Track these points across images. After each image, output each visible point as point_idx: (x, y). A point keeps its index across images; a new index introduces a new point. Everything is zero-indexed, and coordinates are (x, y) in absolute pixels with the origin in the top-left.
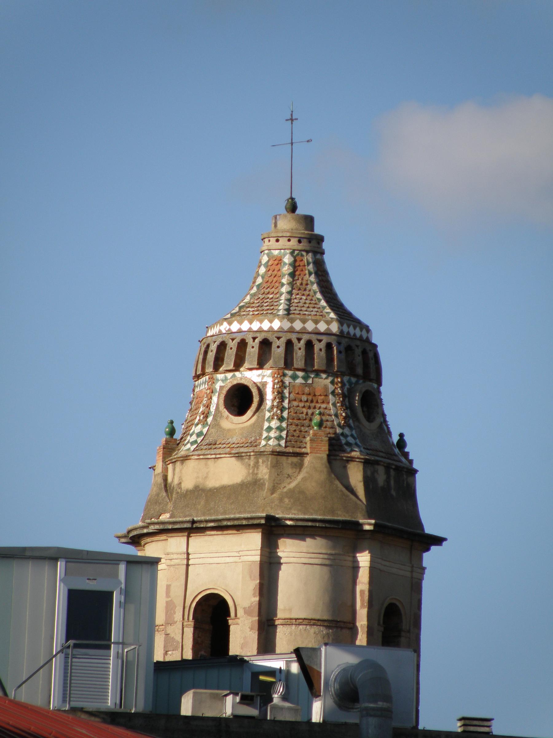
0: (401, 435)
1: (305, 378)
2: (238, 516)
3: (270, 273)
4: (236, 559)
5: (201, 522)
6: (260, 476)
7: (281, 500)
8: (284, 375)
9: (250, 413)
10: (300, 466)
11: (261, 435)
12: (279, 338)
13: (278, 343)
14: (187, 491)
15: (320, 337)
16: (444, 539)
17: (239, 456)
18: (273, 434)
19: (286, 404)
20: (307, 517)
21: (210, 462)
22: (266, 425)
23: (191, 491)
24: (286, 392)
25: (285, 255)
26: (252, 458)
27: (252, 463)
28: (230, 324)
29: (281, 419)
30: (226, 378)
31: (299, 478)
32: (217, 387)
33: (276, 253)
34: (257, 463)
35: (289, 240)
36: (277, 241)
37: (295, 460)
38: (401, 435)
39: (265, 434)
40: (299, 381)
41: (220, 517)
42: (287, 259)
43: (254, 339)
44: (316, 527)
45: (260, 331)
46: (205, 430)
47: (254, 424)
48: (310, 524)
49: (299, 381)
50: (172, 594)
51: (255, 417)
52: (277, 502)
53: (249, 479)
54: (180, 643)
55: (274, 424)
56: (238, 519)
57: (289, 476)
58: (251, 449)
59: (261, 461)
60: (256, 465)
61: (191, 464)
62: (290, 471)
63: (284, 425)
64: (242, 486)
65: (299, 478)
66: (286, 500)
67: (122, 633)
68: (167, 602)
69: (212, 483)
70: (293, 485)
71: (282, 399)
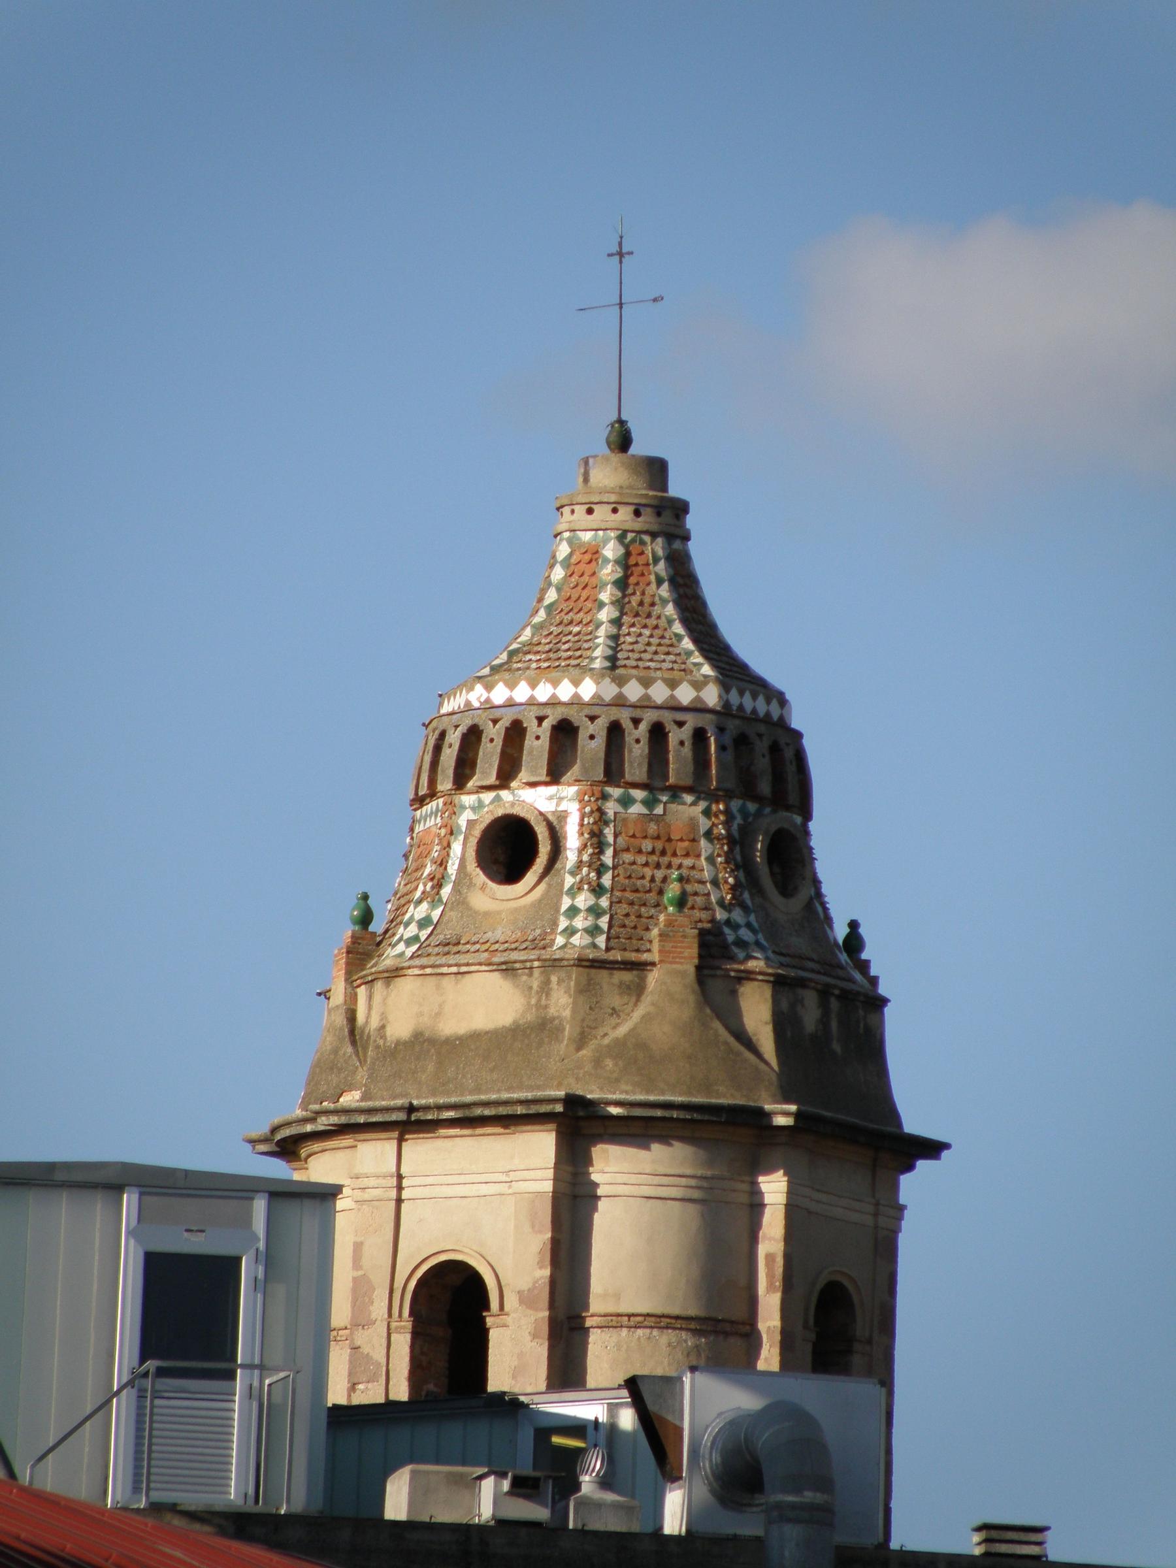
1: (649, 803)
2: (505, 1096)
4: (503, 1188)
6: (552, 1011)
7: (597, 1062)
9: (531, 877)
10: (638, 990)
11: (555, 923)
12: (592, 718)
13: (591, 728)
14: (398, 1043)
15: (680, 716)
17: (508, 969)
20: (652, 1098)
21: (446, 981)
22: (566, 903)
23: (405, 1043)
24: (609, 832)
25: (605, 541)
26: (536, 973)
27: (535, 985)
28: (489, 688)
29: (598, 890)
30: (481, 804)
31: (637, 1014)
32: (462, 821)
33: (587, 536)
34: (547, 982)
35: (615, 511)
36: (590, 511)
37: (627, 976)
39: (563, 923)
40: (637, 809)
41: (469, 1099)
42: (611, 551)
43: (541, 720)
45: (554, 703)
47: (540, 901)
49: (637, 809)
50: (365, 1262)
51: (542, 886)
52: (588, 1067)
56: (506, 1103)
57: (614, 1012)
58: (533, 955)
59: (554, 979)
60: (545, 988)
61: (406, 986)
62: (616, 1000)
63: (604, 902)
64: (516, 1032)
65: (637, 1014)
66: (609, 1063)
68: (355, 1280)
69: (451, 1027)
70: (622, 1030)
71: (600, 847)
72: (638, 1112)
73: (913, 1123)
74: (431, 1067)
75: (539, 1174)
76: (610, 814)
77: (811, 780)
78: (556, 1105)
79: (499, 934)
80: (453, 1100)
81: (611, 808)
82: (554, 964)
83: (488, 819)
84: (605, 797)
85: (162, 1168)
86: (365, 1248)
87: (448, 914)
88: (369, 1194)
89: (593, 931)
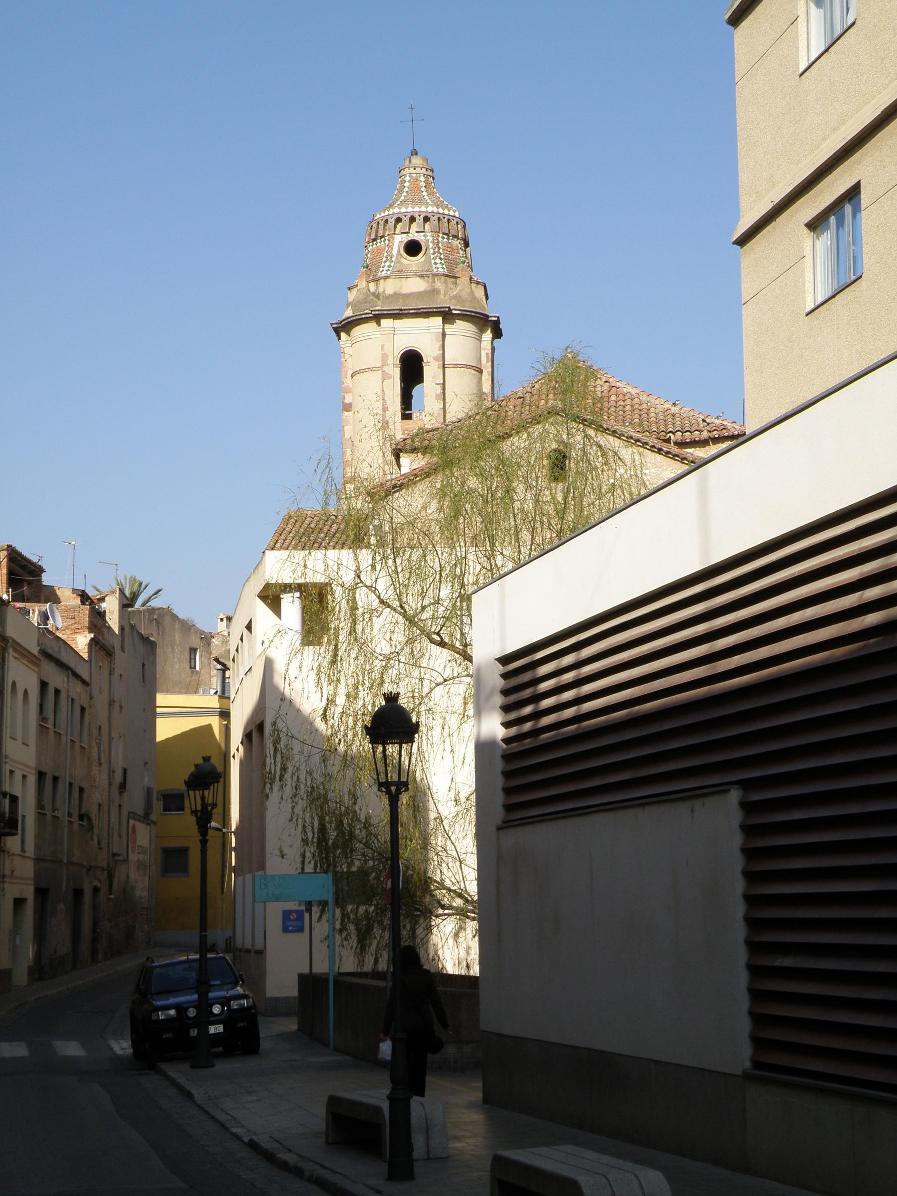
3: (412, 186)
4: (426, 331)
6: (436, 287)
9: (420, 255)
11: (432, 267)
12: (434, 216)
13: (434, 218)
14: (389, 295)
15: (444, 216)
17: (422, 276)
18: (438, 266)
20: (463, 309)
22: (433, 261)
23: (392, 295)
25: (420, 176)
26: (430, 277)
28: (400, 208)
33: (414, 175)
35: (415, 169)
36: (415, 169)
37: (453, 280)
43: (420, 216)
44: (385, 314)
45: (393, 214)
48: (469, 313)
51: (424, 258)
59: (436, 279)
60: (433, 281)
62: (452, 286)
63: (443, 262)
64: (425, 292)
66: (453, 300)
67: (763, 428)
68: (382, 354)
70: (455, 293)
75: (485, 339)
76: (440, 240)
85: (868, 536)
86: (385, 347)
87: (396, 265)
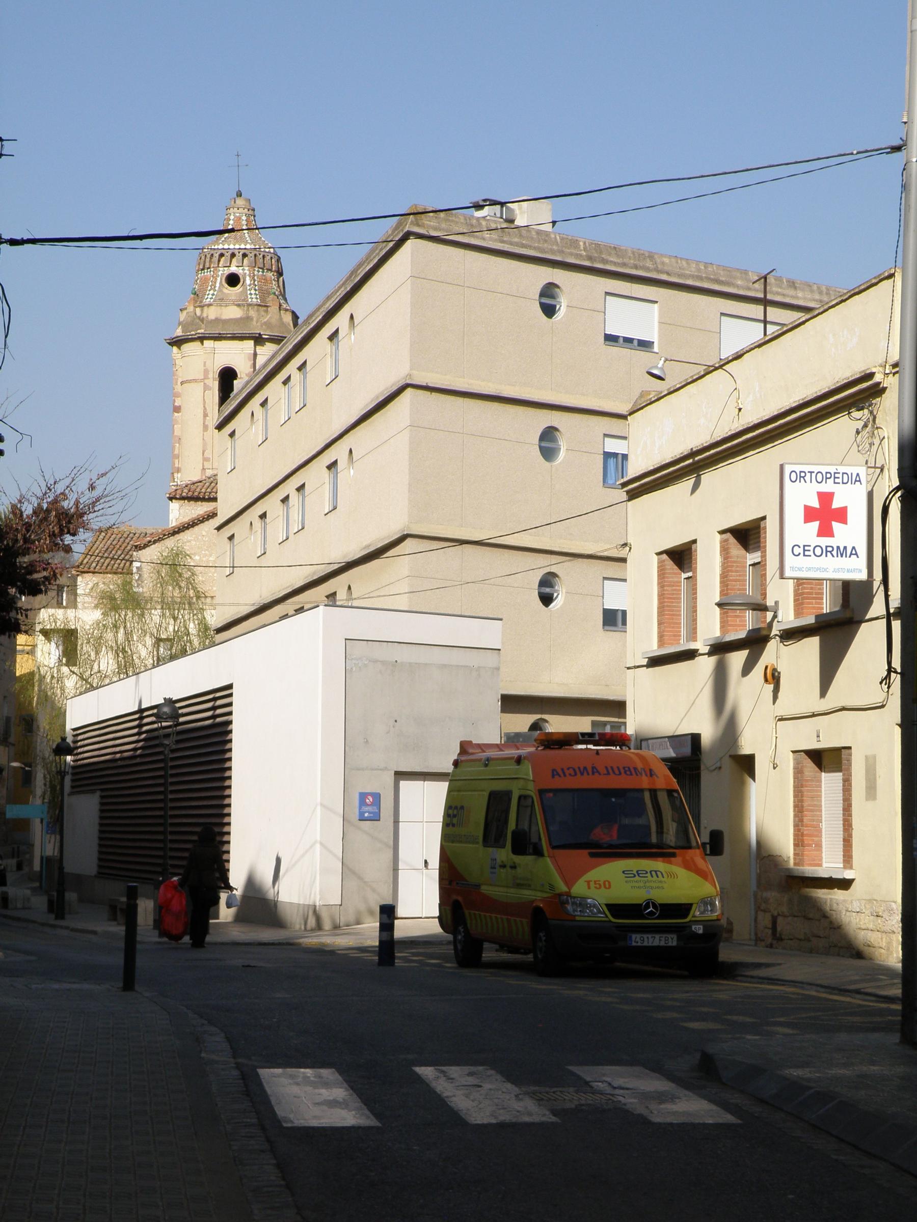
0: (777, 603)
1: (263, 272)
2: (244, 332)
5: (224, 334)
6: (250, 315)
7: (262, 326)
8: (254, 270)
9: (239, 286)
10: (267, 311)
11: (247, 297)
14: (212, 320)
16: (266, 512)
17: (238, 305)
19: (256, 283)
21: (223, 307)
22: (249, 292)
24: (256, 278)
25: (242, 216)
27: (245, 309)
29: (255, 290)
30: (224, 270)
31: (268, 317)
32: (220, 273)
33: (238, 215)
34: (248, 308)
37: (265, 308)
38: (777, 603)
39: (249, 296)
40: (260, 273)
41: (235, 332)
42: (244, 218)
46: (215, 293)
47: (241, 292)
49: (260, 273)
50: (207, 365)
51: (241, 289)
52: (260, 327)
53: (245, 316)
54: (593, 263)
55: (253, 292)
56: (252, 334)
57: (263, 316)
58: (244, 303)
60: (248, 310)
61: (212, 308)
62: (263, 313)
64: (241, 319)
65: (268, 317)
69: (224, 317)
70: (266, 320)
71: (255, 281)
72: (272, 337)
73: (182, 348)
74: (221, 326)
77: (519, 261)
78: (181, 334)
79: (233, 298)
80: (231, 332)
81: (256, 273)
82: (249, 305)
83: (227, 273)
84: (254, 270)
88: (207, 352)
89: (211, 298)
